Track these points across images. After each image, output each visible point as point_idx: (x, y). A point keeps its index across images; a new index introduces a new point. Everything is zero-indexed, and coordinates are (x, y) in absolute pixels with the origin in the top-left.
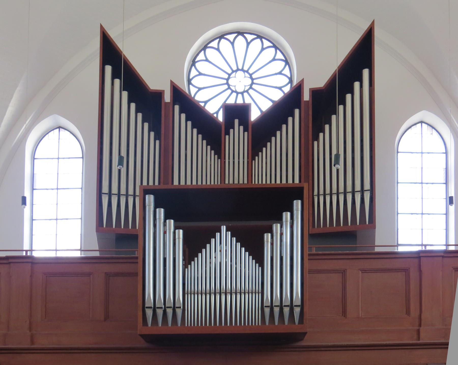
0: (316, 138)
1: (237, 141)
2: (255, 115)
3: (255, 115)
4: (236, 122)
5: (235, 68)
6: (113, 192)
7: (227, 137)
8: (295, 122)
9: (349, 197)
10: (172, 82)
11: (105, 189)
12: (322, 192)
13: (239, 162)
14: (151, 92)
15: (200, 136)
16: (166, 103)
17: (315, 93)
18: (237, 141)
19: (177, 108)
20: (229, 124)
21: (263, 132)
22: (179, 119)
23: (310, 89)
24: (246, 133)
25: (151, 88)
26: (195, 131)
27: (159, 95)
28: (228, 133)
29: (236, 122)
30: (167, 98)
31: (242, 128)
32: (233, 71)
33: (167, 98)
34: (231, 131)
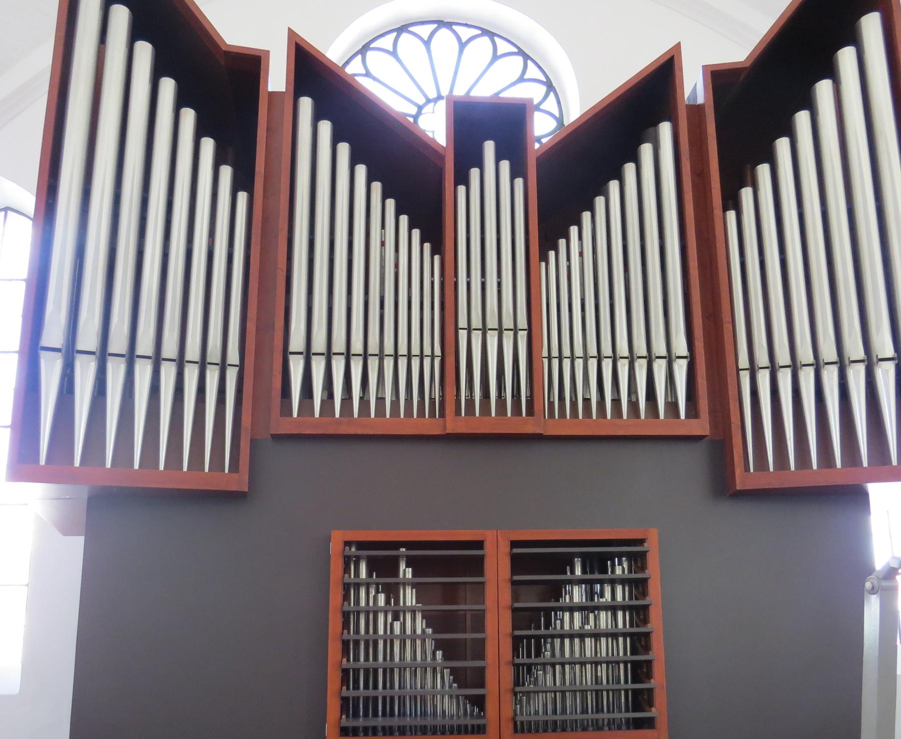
0: (732, 201)
1: (493, 202)
2: (542, 128)
3: (542, 128)
4: (489, 148)
5: (433, 95)
6: (400, 353)
7: (462, 189)
8: (660, 156)
9: (607, 366)
10: (291, 34)
11: (54, 333)
12: (762, 358)
13: (469, 275)
14: (225, 52)
15: (377, 187)
16: (272, 95)
17: (719, 78)
18: (493, 202)
19: (306, 104)
20: (467, 156)
21: (575, 174)
22: (314, 139)
23: (705, 68)
24: (519, 182)
25: (229, 42)
26: (361, 171)
27: (251, 65)
28: (462, 178)
29: (489, 148)
30: (277, 78)
31: (505, 165)
32: (429, 101)
33: (277, 78)
34: (475, 173)
